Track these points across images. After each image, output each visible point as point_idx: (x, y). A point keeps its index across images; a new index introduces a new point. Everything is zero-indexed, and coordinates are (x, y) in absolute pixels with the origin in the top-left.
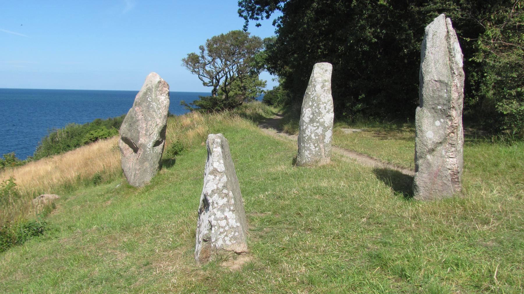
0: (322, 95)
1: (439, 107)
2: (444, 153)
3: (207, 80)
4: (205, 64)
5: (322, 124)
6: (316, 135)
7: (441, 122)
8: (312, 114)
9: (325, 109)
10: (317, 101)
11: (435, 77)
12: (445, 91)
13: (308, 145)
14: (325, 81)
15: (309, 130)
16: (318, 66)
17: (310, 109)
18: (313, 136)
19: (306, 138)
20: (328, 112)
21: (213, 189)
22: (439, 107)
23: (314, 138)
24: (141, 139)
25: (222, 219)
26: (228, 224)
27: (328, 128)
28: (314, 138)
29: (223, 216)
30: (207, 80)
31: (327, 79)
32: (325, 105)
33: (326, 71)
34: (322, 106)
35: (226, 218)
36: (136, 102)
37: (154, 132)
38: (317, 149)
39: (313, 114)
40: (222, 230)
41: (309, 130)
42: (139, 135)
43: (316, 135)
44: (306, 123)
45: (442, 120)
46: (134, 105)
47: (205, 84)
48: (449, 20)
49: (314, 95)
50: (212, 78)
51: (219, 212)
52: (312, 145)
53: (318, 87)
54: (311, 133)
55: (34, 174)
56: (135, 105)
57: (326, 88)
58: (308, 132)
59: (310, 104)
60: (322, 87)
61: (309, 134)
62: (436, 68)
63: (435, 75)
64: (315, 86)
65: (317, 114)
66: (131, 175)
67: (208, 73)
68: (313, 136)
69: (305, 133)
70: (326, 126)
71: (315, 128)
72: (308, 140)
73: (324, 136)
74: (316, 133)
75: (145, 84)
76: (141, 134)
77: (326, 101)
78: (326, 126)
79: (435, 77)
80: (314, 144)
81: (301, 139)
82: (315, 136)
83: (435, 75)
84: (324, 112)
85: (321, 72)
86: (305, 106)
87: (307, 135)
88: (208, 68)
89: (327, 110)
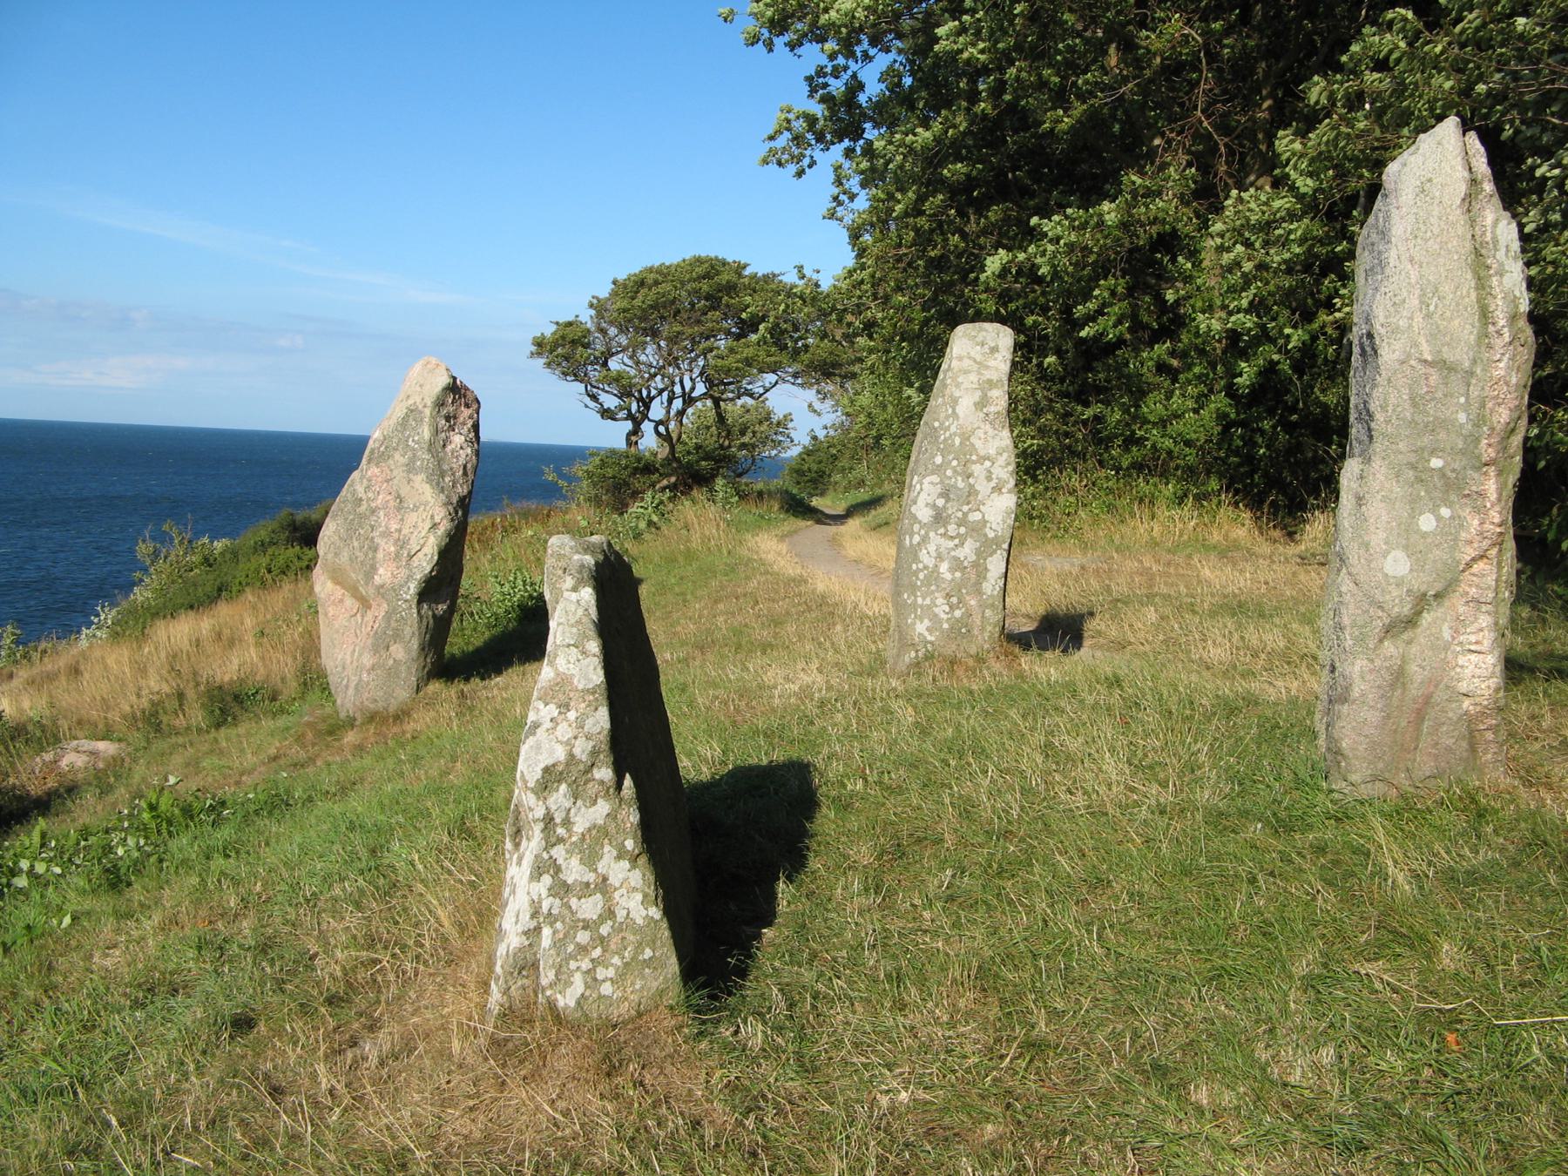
0: (980, 433)
1: (1436, 463)
2: (1447, 634)
3: (611, 401)
4: (609, 354)
5: (977, 529)
6: (957, 565)
7: (1439, 518)
8: (941, 495)
9: (989, 479)
10: (966, 455)
11: (1425, 347)
12: (1462, 400)
13: (928, 601)
14: (991, 384)
15: (932, 548)
16: (965, 335)
17: (935, 478)
18: (944, 567)
19: (921, 576)
20: (998, 489)
21: (550, 762)
22: (1436, 463)
23: (948, 576)
24: (381, 571)
25: (585, 889)
26: (610, 913)
27: (996, 541)
28: (948, 576)
29: (591, 877)
30: (611, 401)
31: (995, 378)
32: (988, 464)
33: (994, 350)
34: (977, 469)
35: (603, 885)
36: (372, 452)
37: (425, 550)
38: (958, 613)
39: (945, 495)
40: (583, 937)
41: (932, 548)
42: (374, 558)
43: (957, 565)
44: (923, 526)
45: (1445, 512)
46: (364, 461)
47: (607, 414)
48: (1472, 138)
49: (953, 429)
50: (625, 393)
51: (575, 862)
52: (940, 601)
53: (966, 405)
54: (940, 557)
55: (108, 670)
56: (369, 462)
57: (992, 409)
58: (927, 558)
59: (938, 460)
60: (981, 404)
61: (930, 562)
62: (1429, 316)
63: (1422, 340)
64: (955, 401)
65: (960, 496)
66: (347, 687)
67: (618, 379)
68: (944, 567)
69: (916, 559)
70: (991, 535)
71: (951, 544)
72: (928, 581)
73: (980, 570)
74: (956, 559)
75: (402, 396)
76: (380, 555)
77: (992, 452)
78: (991, 535)
79: (1425, 347)
80: (948, 596)
81: (905, 581)
82: (952, 570)
83: (1422, 340)
84: (983, 487)
85: (976, 352)
86: (921, 470)
87: (926, 567)
88: (614, 364)
89: (993, 484)
